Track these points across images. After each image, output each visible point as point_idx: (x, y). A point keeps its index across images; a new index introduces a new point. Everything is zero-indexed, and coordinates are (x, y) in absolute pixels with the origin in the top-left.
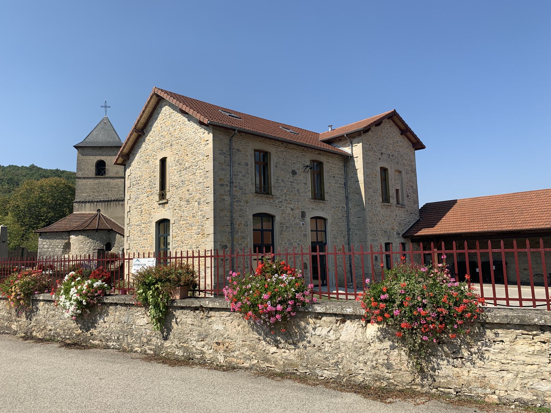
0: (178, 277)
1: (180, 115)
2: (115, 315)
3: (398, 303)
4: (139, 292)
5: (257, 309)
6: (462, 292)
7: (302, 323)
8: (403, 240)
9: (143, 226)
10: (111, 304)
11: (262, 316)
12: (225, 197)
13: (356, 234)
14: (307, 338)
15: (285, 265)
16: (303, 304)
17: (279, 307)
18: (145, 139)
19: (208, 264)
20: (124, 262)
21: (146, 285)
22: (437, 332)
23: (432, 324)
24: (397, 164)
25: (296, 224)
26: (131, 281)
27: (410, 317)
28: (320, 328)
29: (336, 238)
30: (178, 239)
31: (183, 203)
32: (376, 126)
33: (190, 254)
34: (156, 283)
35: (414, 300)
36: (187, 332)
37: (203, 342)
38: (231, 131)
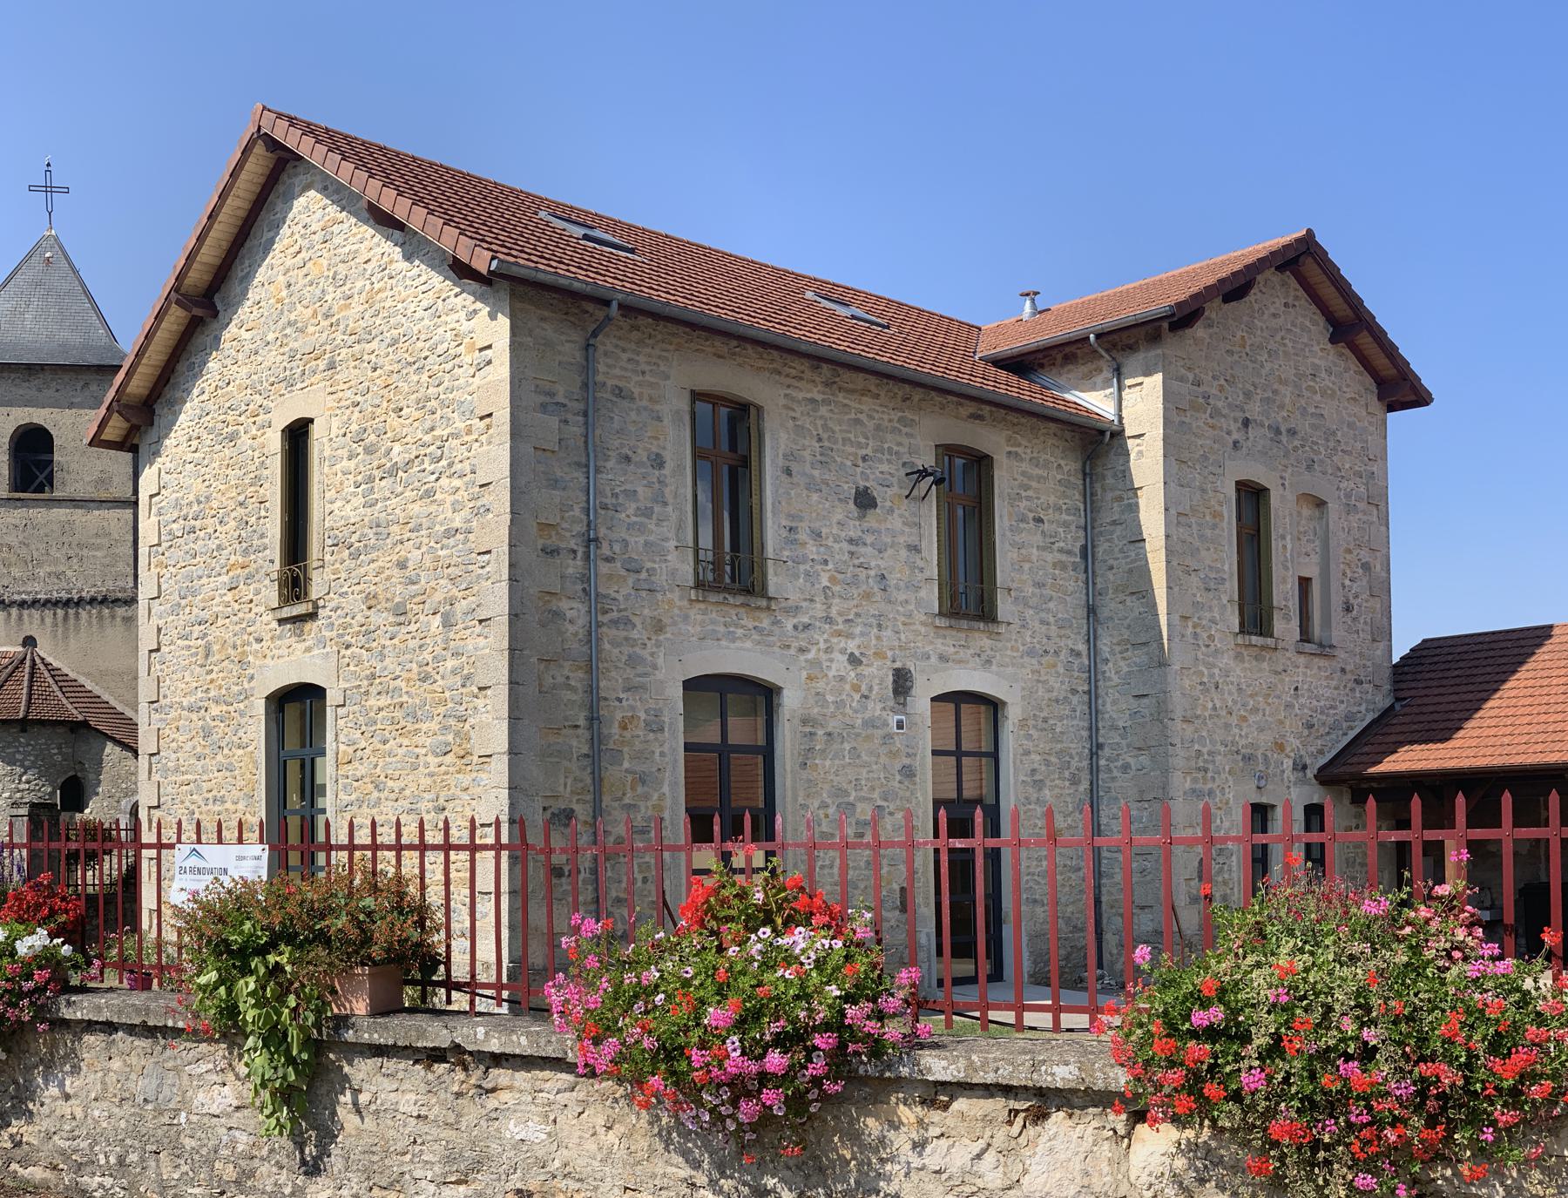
0: (359, 925)
1: (367, 231)
2: (107, 1071)
3: (1260, 1040)
4: (202, 980)
5: (683, 1066)
6: (1525, 999)
7: (871, 1121)
8: (1316, 795)
9: (215, 710)
10: (90, 1026)
11: (706, 1097)
12: (564, 605)
13: (1126, 768)
14: (889, 1180)
15: (802, 889)
16: (877, 1048)
17: (775, 1060)
18: (218, 339)
19: (485, 882)
20: (138, 857)
21: (230, 953)
22: (1412, 1159)
23: (1393, 1125)
24: (1309, 468)
25: (870, 723)
26: (170, 936)
27: (1308, 1099)
28: (943, 1141)
29: (1039, 785)
30: (361, 769)
31: (379, 618)
32: (1228, 298)
33: (410, 835)
34: (272, 946)
35: (1328, 1028)
36: (400, 1146)
37: (462, 1188)
38: (590, 307)
